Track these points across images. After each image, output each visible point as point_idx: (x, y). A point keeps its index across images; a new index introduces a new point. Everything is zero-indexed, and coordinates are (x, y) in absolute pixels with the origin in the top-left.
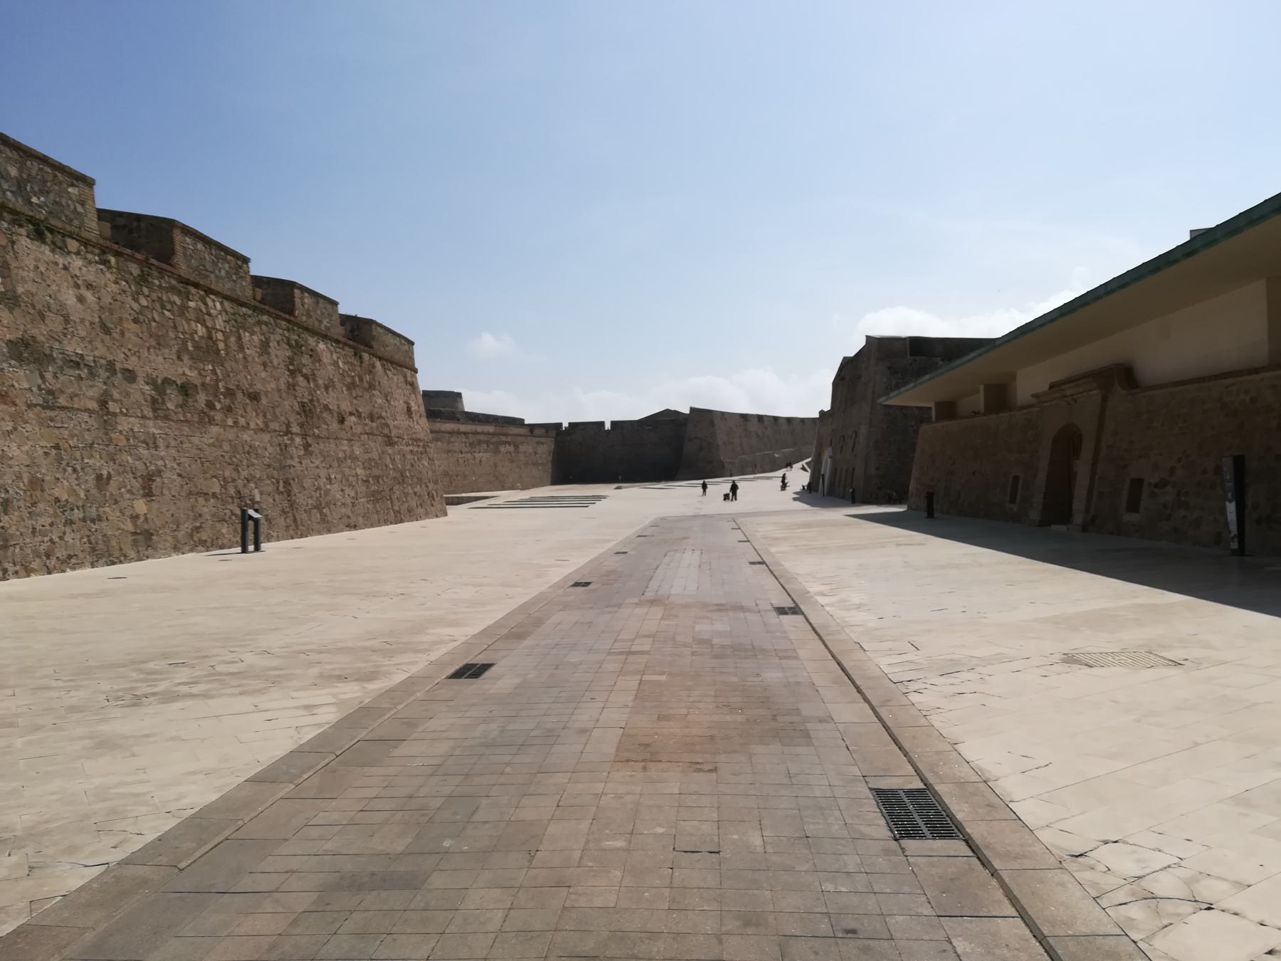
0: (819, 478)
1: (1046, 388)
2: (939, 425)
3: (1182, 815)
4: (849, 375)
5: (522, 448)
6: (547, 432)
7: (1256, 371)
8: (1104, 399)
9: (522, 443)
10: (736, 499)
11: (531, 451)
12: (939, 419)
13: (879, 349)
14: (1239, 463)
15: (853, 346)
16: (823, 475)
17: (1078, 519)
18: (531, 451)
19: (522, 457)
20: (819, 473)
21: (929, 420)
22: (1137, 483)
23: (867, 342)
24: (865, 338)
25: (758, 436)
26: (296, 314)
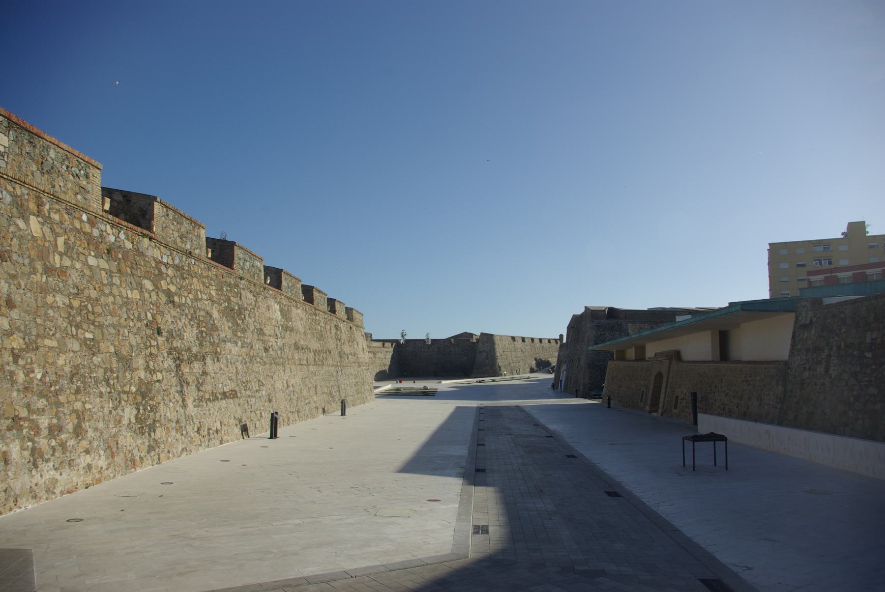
0: (559, 382)
1: (653, 355)
2: (616, 362)
3: (788, 585)
4: (576, 324)
5: (379, 355)
6: (383, 345)
7: (705, 362)
8: (670, 363)
9: (378, 352)
10: (376, 397)
11: (383, 357)
12: (617, 360)
13: (591, 315)
14: (694, 395)
15: (580, 311)
16: (561, 381)
17: (660, 410)
18: (383, 357)
19: (378, 361)
20: (559, 379)
21: (612, 359)
22: (677, 397)
23: (585, 310)
24: (584, 308)
25: (522, 350)
26: (154, 230)
